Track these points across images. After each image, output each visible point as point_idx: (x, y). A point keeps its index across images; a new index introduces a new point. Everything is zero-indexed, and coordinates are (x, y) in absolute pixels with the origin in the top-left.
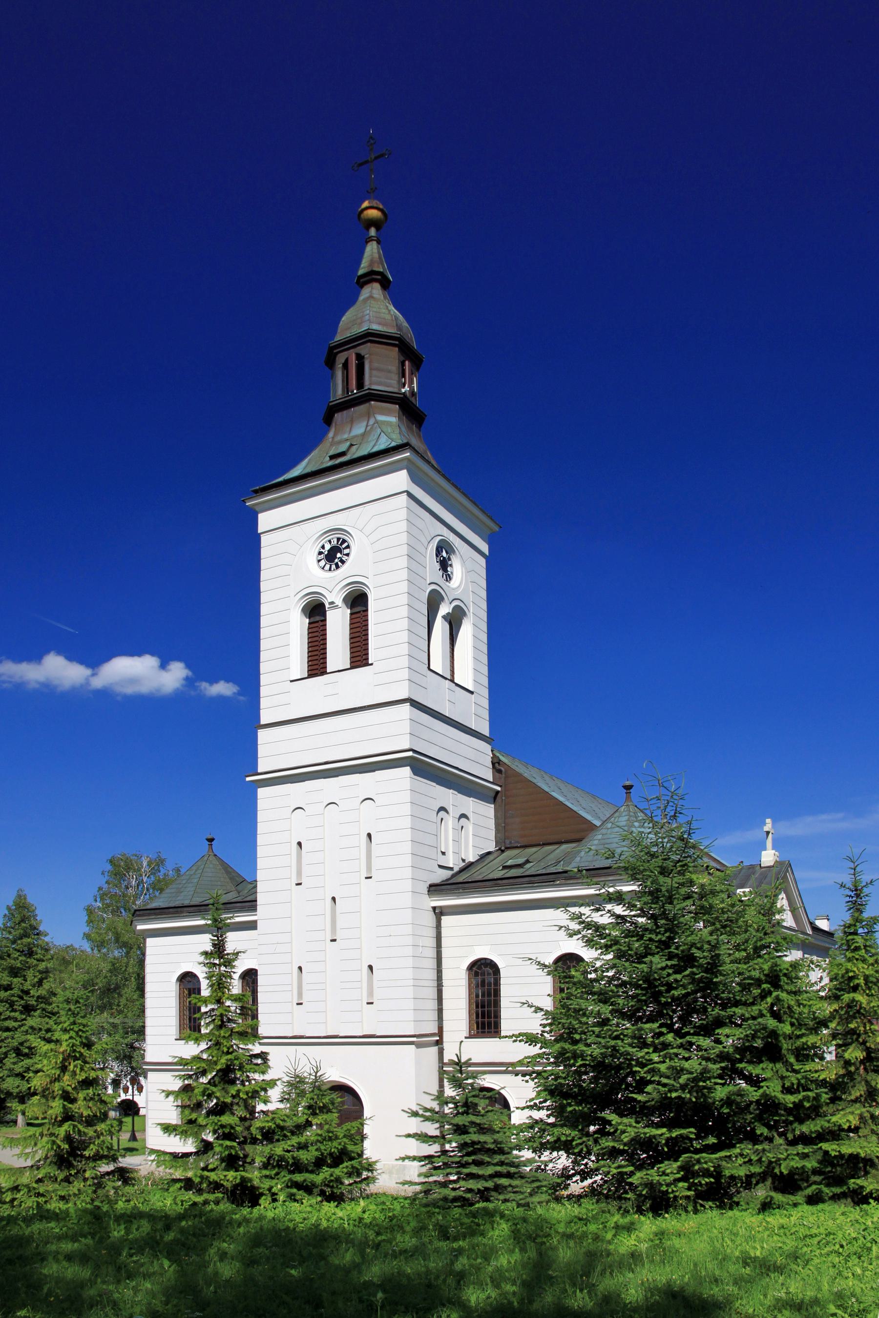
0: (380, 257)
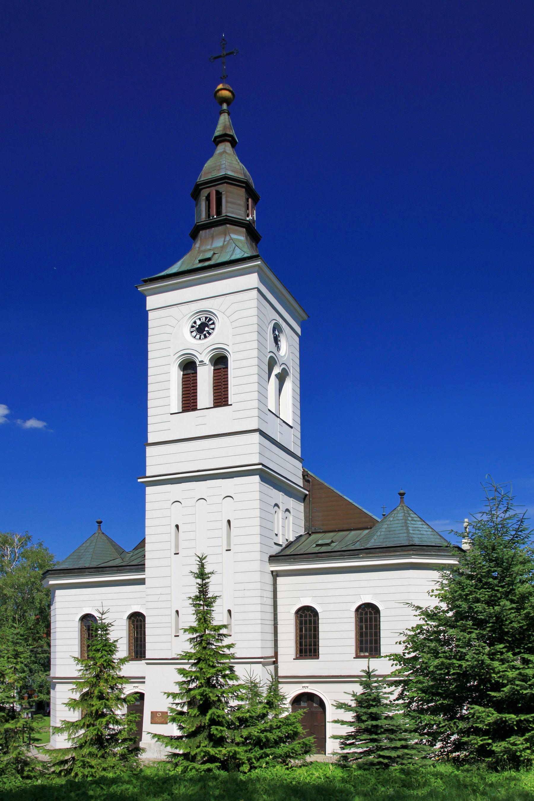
0: (230, 125)
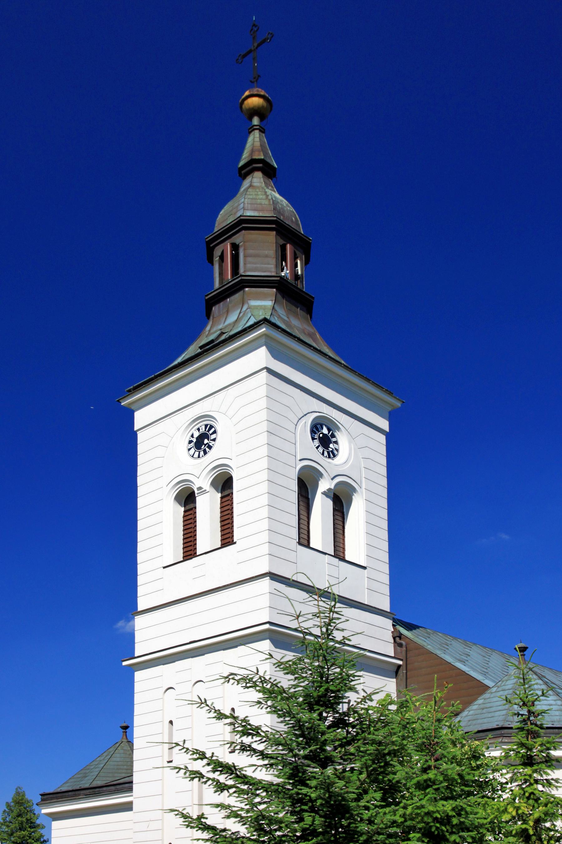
0: (262, 146)
